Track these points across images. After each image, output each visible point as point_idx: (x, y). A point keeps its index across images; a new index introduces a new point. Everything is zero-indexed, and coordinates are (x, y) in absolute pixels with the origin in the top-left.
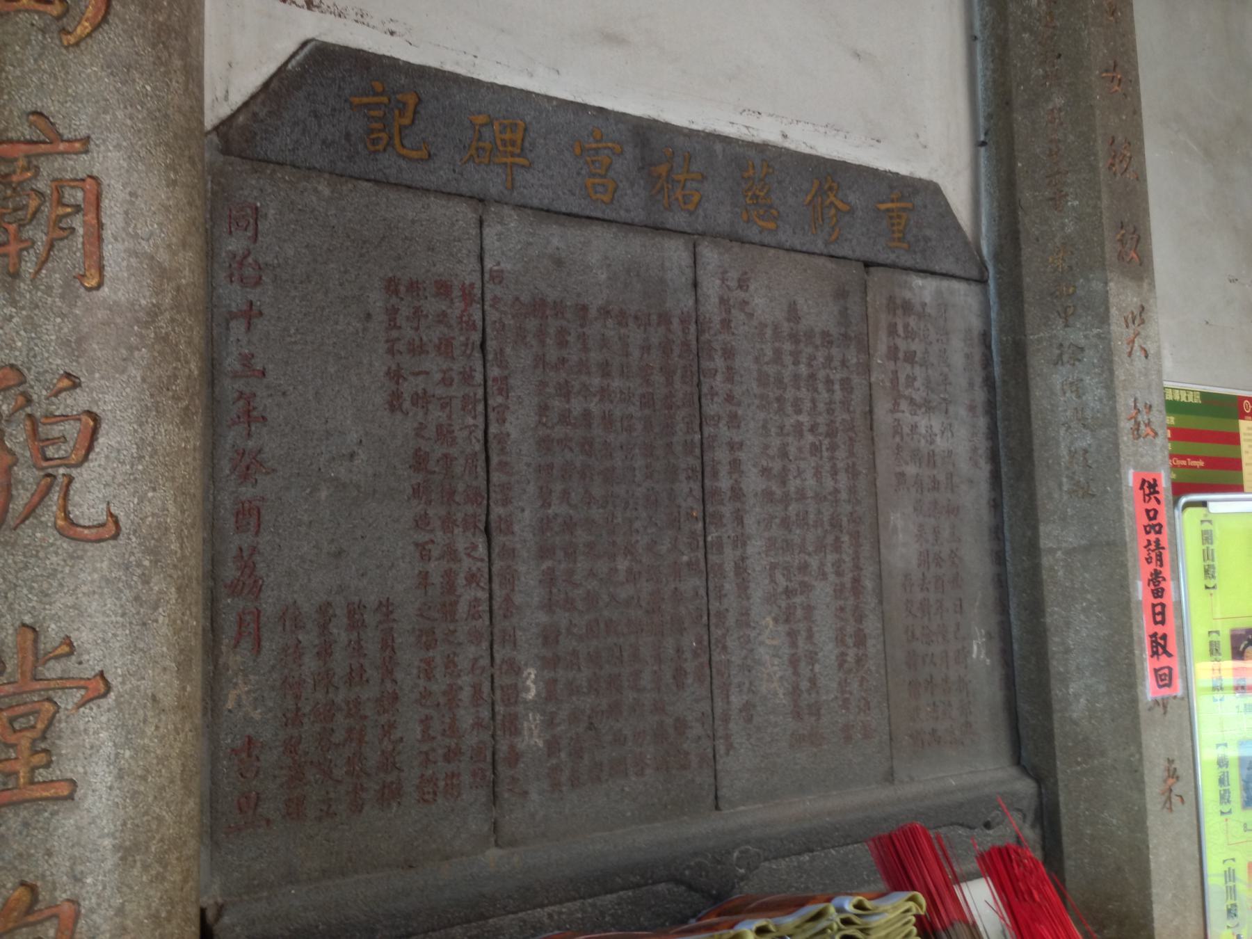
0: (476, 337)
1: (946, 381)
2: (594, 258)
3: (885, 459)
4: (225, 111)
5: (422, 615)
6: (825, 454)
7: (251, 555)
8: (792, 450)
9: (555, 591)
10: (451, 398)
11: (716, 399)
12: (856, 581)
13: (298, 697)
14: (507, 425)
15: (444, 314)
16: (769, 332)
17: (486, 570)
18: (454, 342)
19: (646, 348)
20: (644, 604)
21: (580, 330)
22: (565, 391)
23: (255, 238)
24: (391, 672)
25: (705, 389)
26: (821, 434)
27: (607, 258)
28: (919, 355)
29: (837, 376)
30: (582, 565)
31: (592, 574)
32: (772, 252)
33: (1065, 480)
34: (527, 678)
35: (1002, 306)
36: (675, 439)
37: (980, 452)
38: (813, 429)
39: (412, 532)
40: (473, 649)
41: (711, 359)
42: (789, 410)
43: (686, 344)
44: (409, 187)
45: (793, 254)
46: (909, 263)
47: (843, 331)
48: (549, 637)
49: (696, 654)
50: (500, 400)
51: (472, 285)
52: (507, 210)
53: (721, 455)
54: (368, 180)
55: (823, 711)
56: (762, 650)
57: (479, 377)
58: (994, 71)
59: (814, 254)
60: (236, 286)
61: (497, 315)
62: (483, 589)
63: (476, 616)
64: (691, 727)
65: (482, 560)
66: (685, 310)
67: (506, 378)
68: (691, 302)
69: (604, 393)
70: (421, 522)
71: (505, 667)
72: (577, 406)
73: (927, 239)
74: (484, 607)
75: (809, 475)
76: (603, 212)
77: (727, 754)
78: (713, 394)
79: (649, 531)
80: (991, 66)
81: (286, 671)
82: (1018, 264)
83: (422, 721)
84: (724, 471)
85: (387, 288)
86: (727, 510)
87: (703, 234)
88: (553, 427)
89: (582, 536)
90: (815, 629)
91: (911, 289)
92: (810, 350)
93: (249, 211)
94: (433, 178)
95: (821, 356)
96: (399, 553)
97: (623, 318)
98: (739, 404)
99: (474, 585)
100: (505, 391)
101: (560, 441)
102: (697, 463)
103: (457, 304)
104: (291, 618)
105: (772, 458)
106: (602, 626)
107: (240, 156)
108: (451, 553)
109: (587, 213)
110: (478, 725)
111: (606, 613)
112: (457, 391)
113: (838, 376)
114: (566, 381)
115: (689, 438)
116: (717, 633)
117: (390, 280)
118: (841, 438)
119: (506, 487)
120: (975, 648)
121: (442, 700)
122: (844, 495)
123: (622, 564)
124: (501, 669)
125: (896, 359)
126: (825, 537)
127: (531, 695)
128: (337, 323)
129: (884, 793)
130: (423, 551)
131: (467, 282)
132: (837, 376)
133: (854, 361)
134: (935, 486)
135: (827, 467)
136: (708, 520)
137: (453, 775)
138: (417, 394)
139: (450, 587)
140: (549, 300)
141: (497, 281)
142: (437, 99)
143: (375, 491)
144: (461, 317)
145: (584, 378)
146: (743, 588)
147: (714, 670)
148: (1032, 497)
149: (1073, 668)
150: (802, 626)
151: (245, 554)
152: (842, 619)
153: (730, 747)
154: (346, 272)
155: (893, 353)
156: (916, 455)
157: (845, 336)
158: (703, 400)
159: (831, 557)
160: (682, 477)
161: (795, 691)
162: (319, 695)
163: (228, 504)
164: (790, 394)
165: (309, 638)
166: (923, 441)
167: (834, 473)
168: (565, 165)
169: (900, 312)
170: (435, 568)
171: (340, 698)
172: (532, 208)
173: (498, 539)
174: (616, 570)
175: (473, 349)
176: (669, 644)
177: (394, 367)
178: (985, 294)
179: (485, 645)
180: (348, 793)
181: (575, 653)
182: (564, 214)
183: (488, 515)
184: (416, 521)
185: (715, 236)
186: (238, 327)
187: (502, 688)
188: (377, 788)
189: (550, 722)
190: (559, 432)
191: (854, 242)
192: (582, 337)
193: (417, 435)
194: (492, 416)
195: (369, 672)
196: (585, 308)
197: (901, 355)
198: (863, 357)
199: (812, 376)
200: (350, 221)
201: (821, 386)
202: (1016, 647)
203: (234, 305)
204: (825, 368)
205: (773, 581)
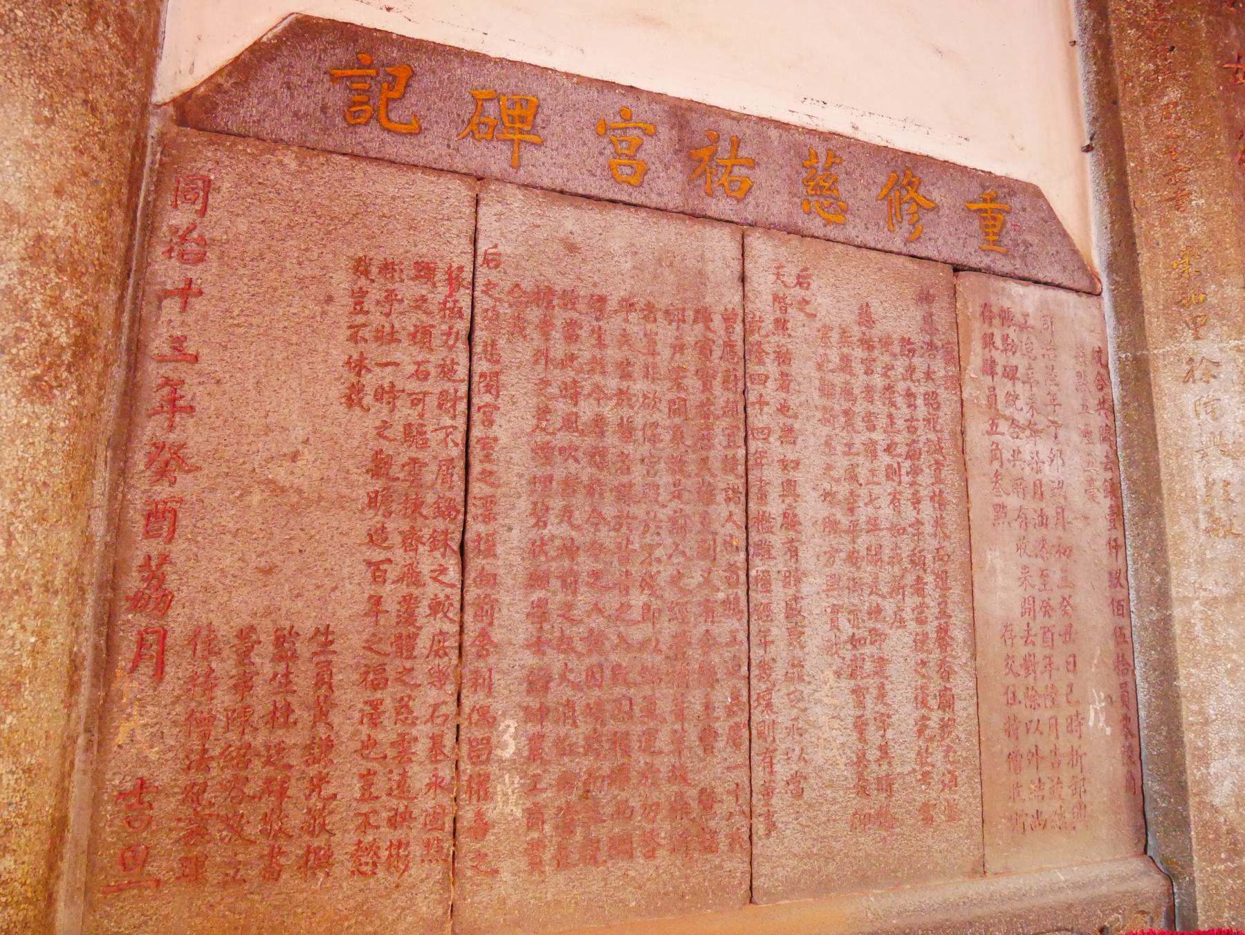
0: (462, 326)
1: (1055, 402)
2: (616, 245)
3: (980, 489)
4: (187, 83)
5: (370, 649)
6: (905, 479)
7: (159, 566)
8: (863, 474)
9: (546, 626)
10: (425, 394)
11: (766, 409)
12: (943, 631)
13: (205, 736)
14: (495, 427)
15: (424, 299)
16: (835, 336)
17: (458, 598)
18: (434, 331)
19: (679, 348)
20: (663, 647)
21: (595, 323)
22: (572, 392)
23: (203, 212)
24: (326, 714)
25: (752, 397)
26: (900, 455)
27: (633, 245)
28: (1021, 371)
29: (920, 390)
30: (584, 598)
31: (597, 609)
32: (839, 248)
33: (1201, 516)
34: (505, 731)
35: (1119, 320)
36: (712, 453)
37: (1098, 484)
38: (888, 449)
39: (364, 548)
40: (433, 692)
41: (761, 362)
42: (860, 425)
43: (729, 345)
44: (392, 162)
45: (865, 251)
46: (1008, 268)
47: (927, 338)
48: (537, 682)
49: (730, 713)
50: (488, 398)
51: (461, 269)
52: (510, 190)
53: (772, 474)
54: (344, 154)
55: (895, 786)
56: (818, 709)
57: (462, 372)
58: (1097, 73)
59: (891, 252)
60: (175, 262)
61: (491, 302)
62: (452, 621)
63: (439, 653)
64: (721, 801)
65: (453, 586)
66: (730, 306)
67: (497, 374)
68: (737, 298)
69: (622, 395)
70: (376, 537)
71: (475, 717)
72: (587, 410)
73: (1027, 245)
74: (452, 642)
75: (884, 502)
76: (630, 195)
77: (768, 835)
78: (762, 402)
79: (675, 560)
80: (1094, 68)
81: (193, 704)
82: (1136, 273)
83: (362, 776)
84: (774, 493)
85: (356, 269)
86: (777, 539)
87: (753, 225)
88: (554, 433)
89: (585, 564)
90: (888, 687)
91: (1009, 297)
92: (886, 358)
93: (200, 183)
94: (422, 153)
95: (900, 365)
96: (346, 571)
97: (649, 311)
98: (795, 417)
99: (440, 615)
100: (494, 386)
101: (562, 450)
102: (740, 483)
103: (440, 289)
104: (203, 641)
105: (838, 481)
106: (608, 672)
107: (195, 127)
108: (411, 576)
109: (610, 195)
110: (436, 784)
111: (613, 657)
112: (434, 386)
113: (922, 390)
114: (575, 382)
115: (730, 453)
116: (759, 687)
117: (360, 260)
118: (925, 461)
119: (489, 501)
120: (1092, 713)
121: (391, 753)
122: (928, 528)
123: (638, 599)
124: (470, 718)
125: (993, 374)
126: (902, 577)
127: (508, 753)
128: (290, 306)
129: (976, 888)
130: (377, 570)
131: (455, 266)
132: (920, 390)
133: (942, 373)
134: (1043, 521)
135: (908, 493)
136: (751, 551)
137: (400, 844)
138: (382, 387)
139: (408, 617)
140: (557, 288)
141: (492, 265)
142: (434, 72)
143: (321, 498)
144: (445, 303)
145: (597, 378)
146: (796, 633)
147: (754, 732)
148: (1161, 534)
149: (1215, 743)
150: (872, 683)
151: (153, 564)
152: (923, 676)
153: (771, 827)
154: (307, 250)
155: (989, 368)
156: (1018, 482)
157: (931, 345)
158: (749, 410)
159: (911, 601)
160: (720, 497)
161: (861, 761)
162: (233, 736)
163: (139, 504)
164: (861, 407)
165: (225, 666)
166: (1027, 469)
167: (916, 502)
168: (584, 144)
169: (997, 321)
170: (391, 593)
171: (259, 741)
172: (542, 188)
173: (476, 563)
174: (630, 606)
175: (456, 340)
176: (695, 701)
177: (356, 356)
178: (1100, 307)
179: (450, 688)
180: (262, 857)
181: (569, 704)
182: (582, 196)
183: (464, 533)
184: (371, 536)
185: (769, 228)
186: (171, 307)
187: (470, 741)
188: (301, 852)
189: (533, 788)
190: (562, 439)
191: (940, 241)
192: (598, 334)
193: (380, 435)
194: (477, 417)
195: (298, 712)
196: (602, 300)
197: (999, 369)
198: (953, 370)
199: (889, 388)
200: (318, 195)
201: (900, 401)
202: (1142, 713)
203: (169, 281)
204: (904, 379)
205: (835, 627)
